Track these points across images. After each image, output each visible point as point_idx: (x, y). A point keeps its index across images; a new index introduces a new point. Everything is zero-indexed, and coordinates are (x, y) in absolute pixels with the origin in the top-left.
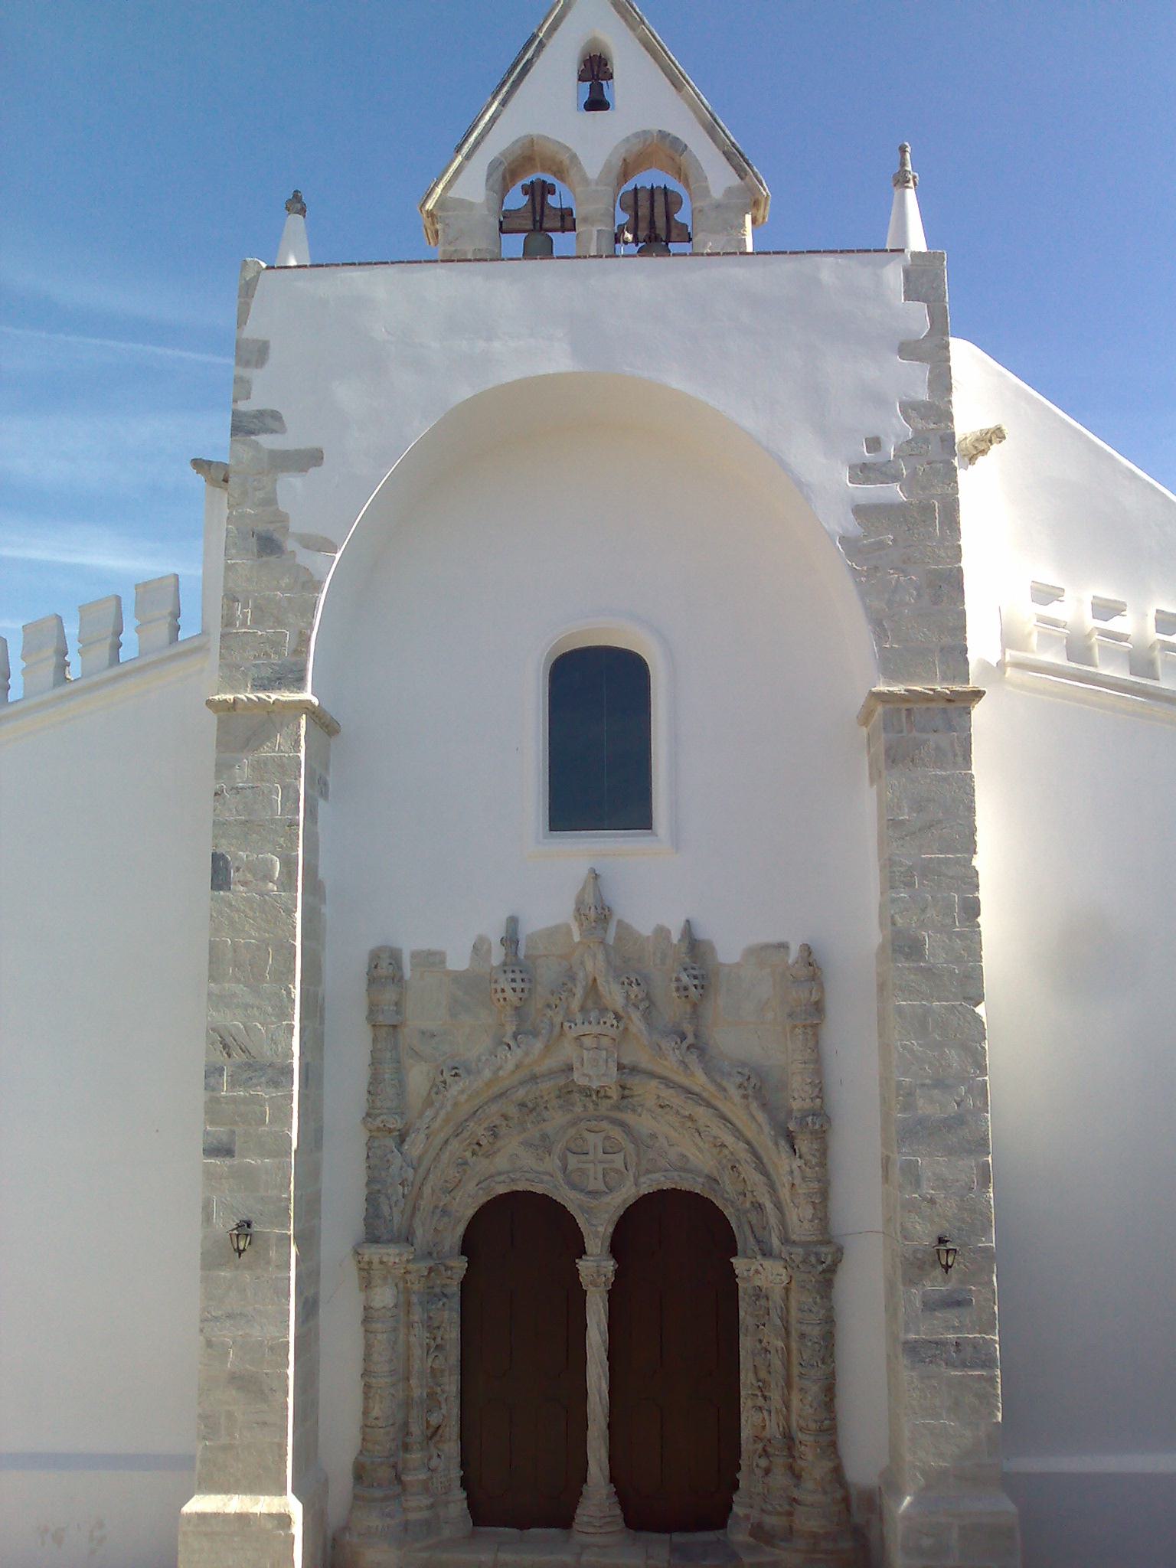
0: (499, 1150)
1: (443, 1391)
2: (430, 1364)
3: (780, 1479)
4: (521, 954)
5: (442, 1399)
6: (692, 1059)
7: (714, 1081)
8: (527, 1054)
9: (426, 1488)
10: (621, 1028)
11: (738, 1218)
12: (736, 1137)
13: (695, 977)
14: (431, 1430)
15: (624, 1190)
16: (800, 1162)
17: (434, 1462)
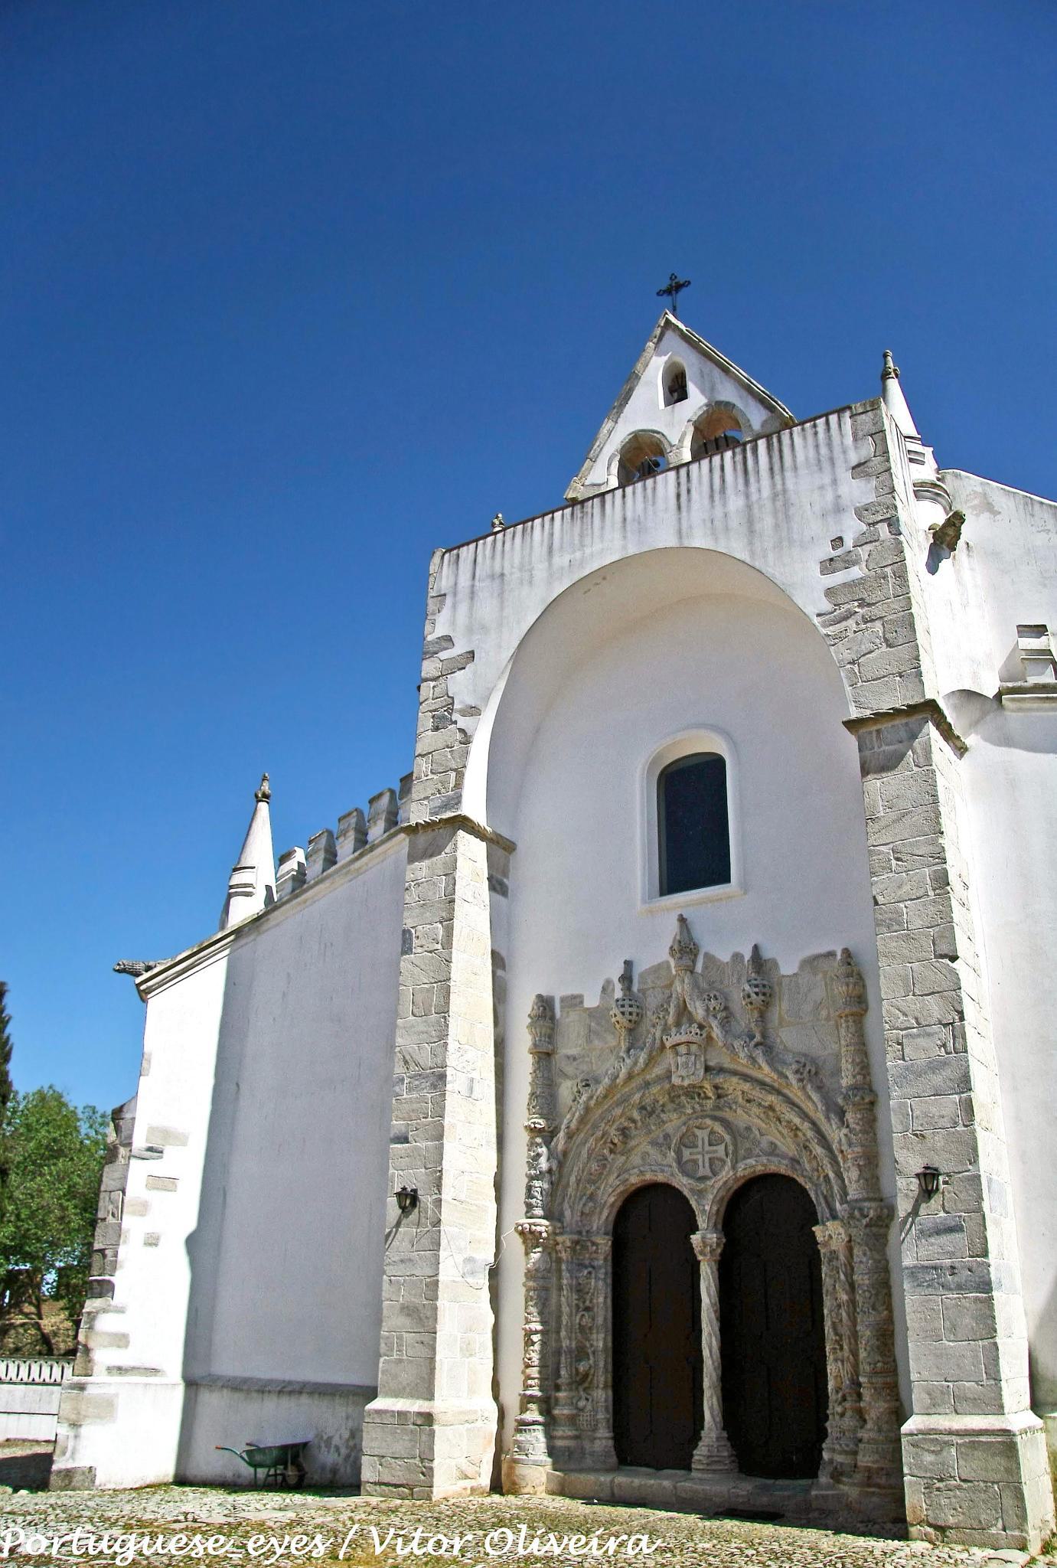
0: (632, 1149)
1: (592, 1345)
2: (578, 1321)
3: (848, 1422)
4: (635, 988)
5: (590, 1351)
6: (759, 1054)
7: (775, 1070)
8: (635, 1063)
9: (572, 1420)
10: (704, 1035)
11: (817, 1194)
12: (801, 1118)
13: (756, 986)
14: (580, 1376)
15: (724, 1173)
16: (845, 1131)
17: (582, 1404)
